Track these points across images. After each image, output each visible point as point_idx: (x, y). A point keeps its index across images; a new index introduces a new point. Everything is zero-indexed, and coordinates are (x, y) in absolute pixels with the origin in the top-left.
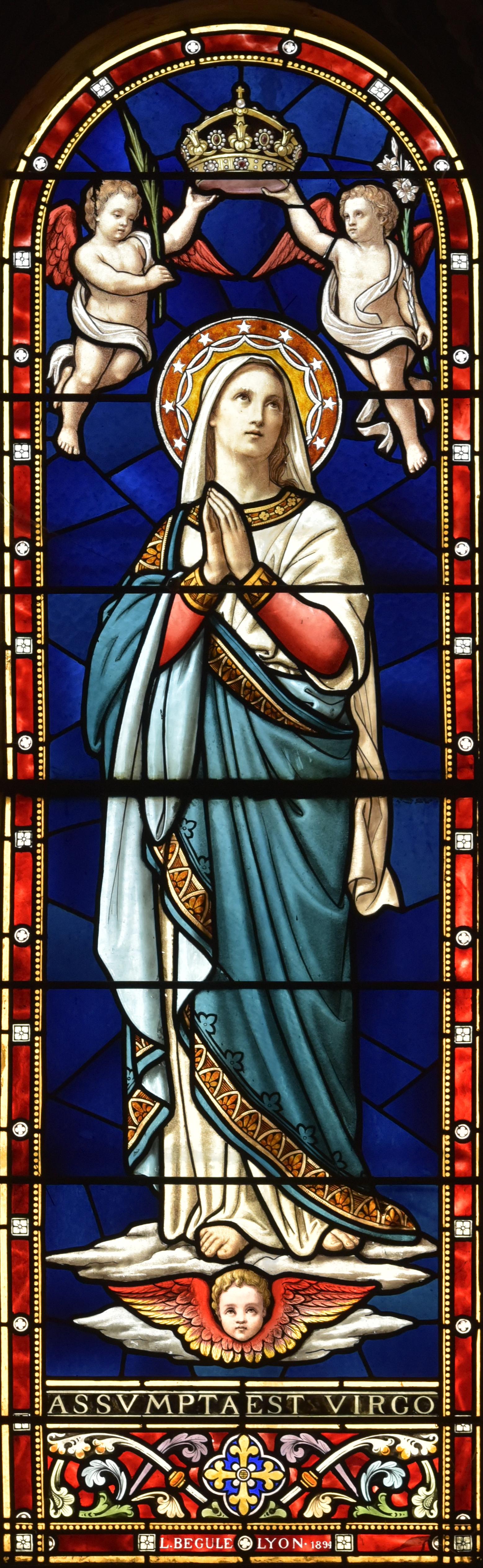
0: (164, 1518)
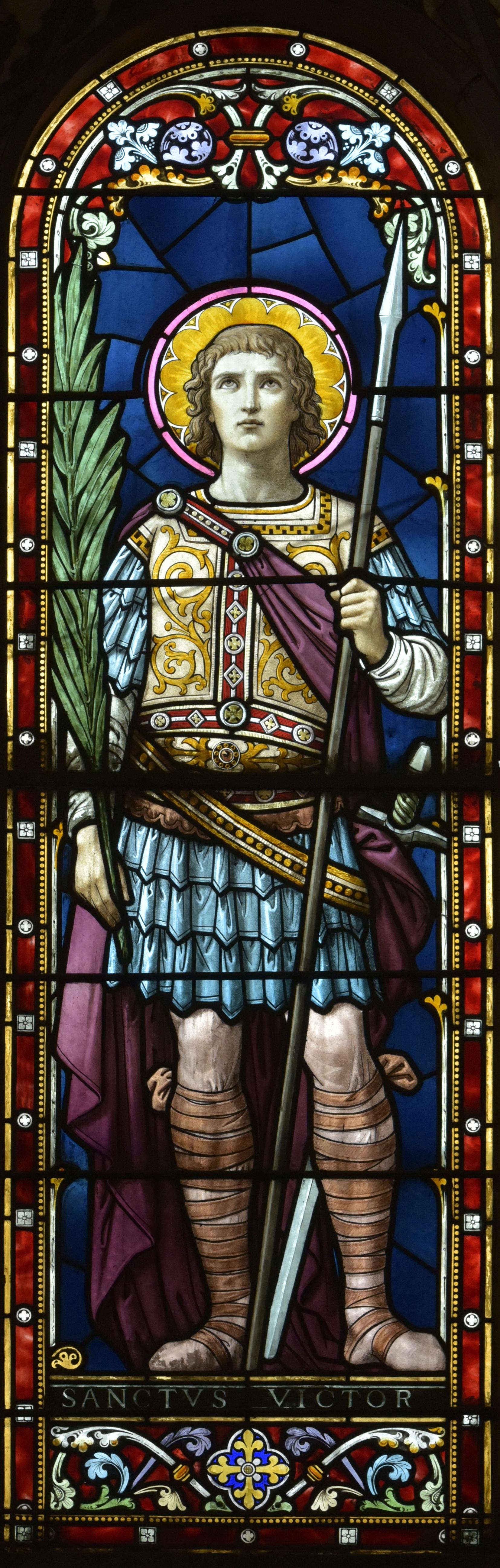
0: (164, 1510)
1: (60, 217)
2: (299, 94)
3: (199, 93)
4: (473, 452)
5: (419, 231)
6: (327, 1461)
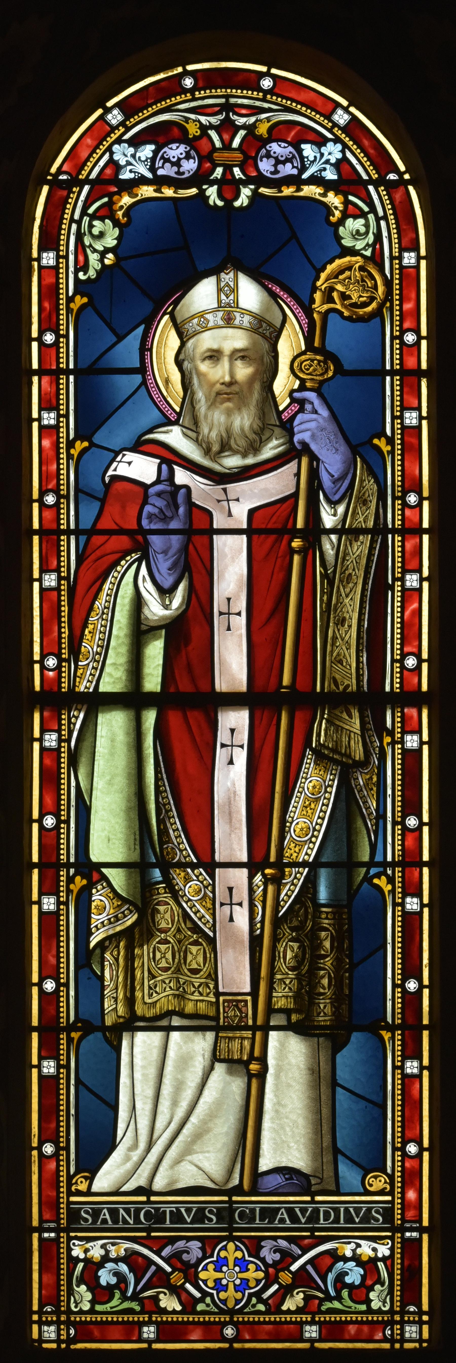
0: (164, 1311)
1: (74, 226)
2: (268, 119)
3: (187, 120)
4: (411, 418)
5: (367, 233)
6: (294, 1268)
